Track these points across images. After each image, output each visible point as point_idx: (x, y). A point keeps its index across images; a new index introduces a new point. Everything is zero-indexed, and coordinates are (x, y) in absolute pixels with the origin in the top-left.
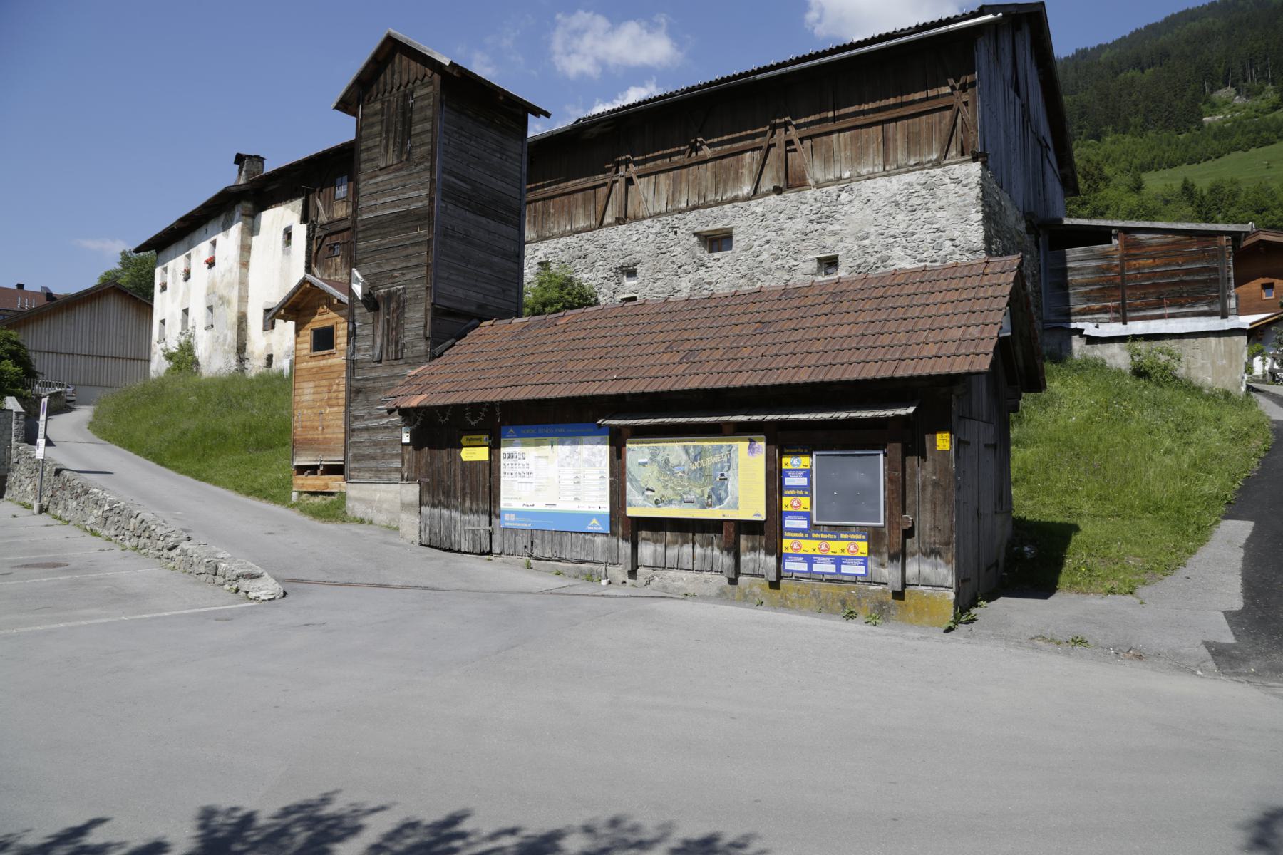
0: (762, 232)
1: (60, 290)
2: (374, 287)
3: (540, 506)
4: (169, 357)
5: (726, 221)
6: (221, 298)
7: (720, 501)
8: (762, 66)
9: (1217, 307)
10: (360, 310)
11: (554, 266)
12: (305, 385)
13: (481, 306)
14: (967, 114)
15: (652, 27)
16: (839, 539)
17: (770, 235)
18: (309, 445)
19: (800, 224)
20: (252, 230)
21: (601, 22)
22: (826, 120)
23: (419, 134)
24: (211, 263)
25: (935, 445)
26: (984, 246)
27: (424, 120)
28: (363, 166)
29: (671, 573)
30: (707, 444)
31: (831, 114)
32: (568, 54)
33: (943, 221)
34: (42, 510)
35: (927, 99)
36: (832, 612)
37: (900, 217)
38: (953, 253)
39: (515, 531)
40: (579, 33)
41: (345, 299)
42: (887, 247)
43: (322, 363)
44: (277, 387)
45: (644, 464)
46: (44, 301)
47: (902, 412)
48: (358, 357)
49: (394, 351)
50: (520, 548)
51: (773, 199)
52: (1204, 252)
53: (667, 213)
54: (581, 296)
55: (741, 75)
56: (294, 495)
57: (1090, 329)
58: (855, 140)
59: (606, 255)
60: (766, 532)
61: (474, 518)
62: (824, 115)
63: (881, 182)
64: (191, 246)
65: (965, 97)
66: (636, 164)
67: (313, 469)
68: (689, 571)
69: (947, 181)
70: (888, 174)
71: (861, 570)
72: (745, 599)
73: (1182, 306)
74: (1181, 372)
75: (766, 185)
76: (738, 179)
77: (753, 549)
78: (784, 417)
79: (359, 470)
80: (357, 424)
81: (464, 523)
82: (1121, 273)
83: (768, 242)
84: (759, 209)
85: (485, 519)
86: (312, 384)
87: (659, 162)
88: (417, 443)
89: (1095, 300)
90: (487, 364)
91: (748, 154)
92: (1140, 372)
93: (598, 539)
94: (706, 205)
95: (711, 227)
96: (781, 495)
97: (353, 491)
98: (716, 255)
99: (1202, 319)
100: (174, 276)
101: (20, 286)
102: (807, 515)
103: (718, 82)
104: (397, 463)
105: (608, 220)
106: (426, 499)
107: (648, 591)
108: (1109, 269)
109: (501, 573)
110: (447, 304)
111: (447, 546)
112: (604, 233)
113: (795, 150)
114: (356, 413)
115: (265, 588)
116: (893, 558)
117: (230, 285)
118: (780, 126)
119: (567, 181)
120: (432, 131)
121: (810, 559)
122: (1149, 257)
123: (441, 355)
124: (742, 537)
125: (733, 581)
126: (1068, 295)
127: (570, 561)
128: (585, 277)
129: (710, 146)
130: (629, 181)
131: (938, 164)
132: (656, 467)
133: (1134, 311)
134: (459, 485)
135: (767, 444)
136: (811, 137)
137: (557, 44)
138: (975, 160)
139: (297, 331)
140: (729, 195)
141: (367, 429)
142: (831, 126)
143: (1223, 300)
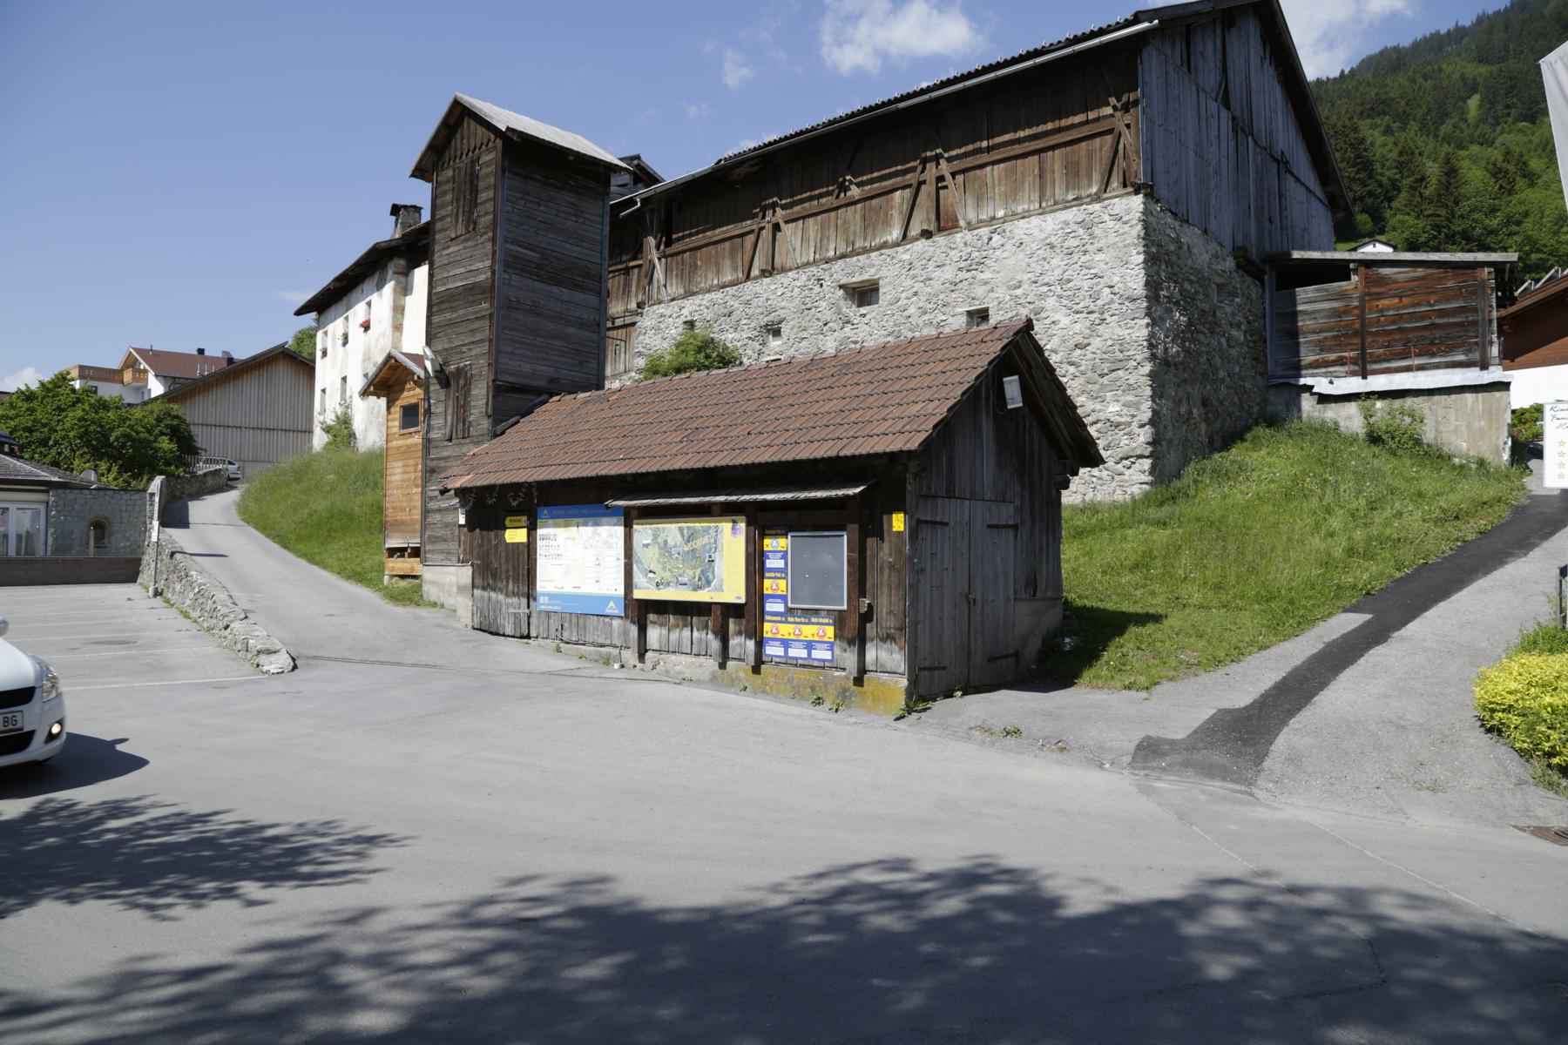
0: (909, 282)
2: (446, 363)
3: (568, 589)
5: (873, 271)
7: (708, 583)
8: (1079, 33)
9: (1476, 356)
11: (698, 324)
13: (552, 380)
14: (1128, 138)
17: (918, 286)
18: (400, 526)
19: (949, 273)
20: (405, 289)
23: (483, 203)
24: (366, 326)
25: (891, 525)
26: (1144, 293)
27: (487, 188)
29: (673, 657)
30: (698, 525)
31: (985, 144)
32: (840, 45)
34: (157, 593)
36: (803, 698)
37: (1054, 262)
38: (1112, 302)
39: (548, 614)
42: (1041, 296)
45: (647, 546)
48: (433, 435)
49: (461, 430)
50: (552, 631)
51: (922, 244)
52: (1460, 288)
53: (815, 262)
55: (884, 104)
57: (1322, 385)
59: (749, 312)
60: (745, 615)
61: (515, 600)
62: (977, 145)
64: (349, 308)
65: (1128, 119)
66: (784, 207)
67: (400, 552)
68: (684, 653)
69: (1106, 218)
71: (827, 655)
72: (732, 684)
73: (1433, 355)
74: (1429, 436)
75: (915, 230)
76: (887, 223)
77: (739, 633)
78: (734, 498)
80: (432, 505)
82: (1362, 317)
83: (916, 294)
84: (906, 257)
85: (524, 601)
86: (400, 464)
87: (807, 205)
88: (471, 525)
89: (1330, 350)
91: (898, 193)
92: (1374, 439)
93: (616, 622)
94: (855, 253)
95: (858, 278)
96: (762, 577)
97: (428, 574)
98: (863, 310)
99: (1458, 371)
100: (334, 341)
101: (201, 351)
102: (784, 598)
104: (453, 546)
105: (755, 272)
106: (478, 581)
107: (654, 675)
108: (1346, 311)
109: (536, 657)
110: (511, 379)
111: (493, 629)
112: (749, 286)
113: (946, 187)
116: (851, 642)
118: (931, 159)
119: (714, 228)
121: (786, 644)
122: (1394, 296)
123: (503, 433)
124: (731, 621)
125: (722, 666)
126: (1297, 345)
127: (593, 644)
128: (730, 338)
129: (859, 185)
130: (777, 228)
131: (1097, 198)
132: (656, 550)
133: (1375, 362)
135: (748, 525)
136: (964, 171)
137: (826, 37)
138: (1137, 192)
139: (388, 408)
140: (877, 241)
141: (440, 510)
142: (985, 158)
143: (1484, 346)
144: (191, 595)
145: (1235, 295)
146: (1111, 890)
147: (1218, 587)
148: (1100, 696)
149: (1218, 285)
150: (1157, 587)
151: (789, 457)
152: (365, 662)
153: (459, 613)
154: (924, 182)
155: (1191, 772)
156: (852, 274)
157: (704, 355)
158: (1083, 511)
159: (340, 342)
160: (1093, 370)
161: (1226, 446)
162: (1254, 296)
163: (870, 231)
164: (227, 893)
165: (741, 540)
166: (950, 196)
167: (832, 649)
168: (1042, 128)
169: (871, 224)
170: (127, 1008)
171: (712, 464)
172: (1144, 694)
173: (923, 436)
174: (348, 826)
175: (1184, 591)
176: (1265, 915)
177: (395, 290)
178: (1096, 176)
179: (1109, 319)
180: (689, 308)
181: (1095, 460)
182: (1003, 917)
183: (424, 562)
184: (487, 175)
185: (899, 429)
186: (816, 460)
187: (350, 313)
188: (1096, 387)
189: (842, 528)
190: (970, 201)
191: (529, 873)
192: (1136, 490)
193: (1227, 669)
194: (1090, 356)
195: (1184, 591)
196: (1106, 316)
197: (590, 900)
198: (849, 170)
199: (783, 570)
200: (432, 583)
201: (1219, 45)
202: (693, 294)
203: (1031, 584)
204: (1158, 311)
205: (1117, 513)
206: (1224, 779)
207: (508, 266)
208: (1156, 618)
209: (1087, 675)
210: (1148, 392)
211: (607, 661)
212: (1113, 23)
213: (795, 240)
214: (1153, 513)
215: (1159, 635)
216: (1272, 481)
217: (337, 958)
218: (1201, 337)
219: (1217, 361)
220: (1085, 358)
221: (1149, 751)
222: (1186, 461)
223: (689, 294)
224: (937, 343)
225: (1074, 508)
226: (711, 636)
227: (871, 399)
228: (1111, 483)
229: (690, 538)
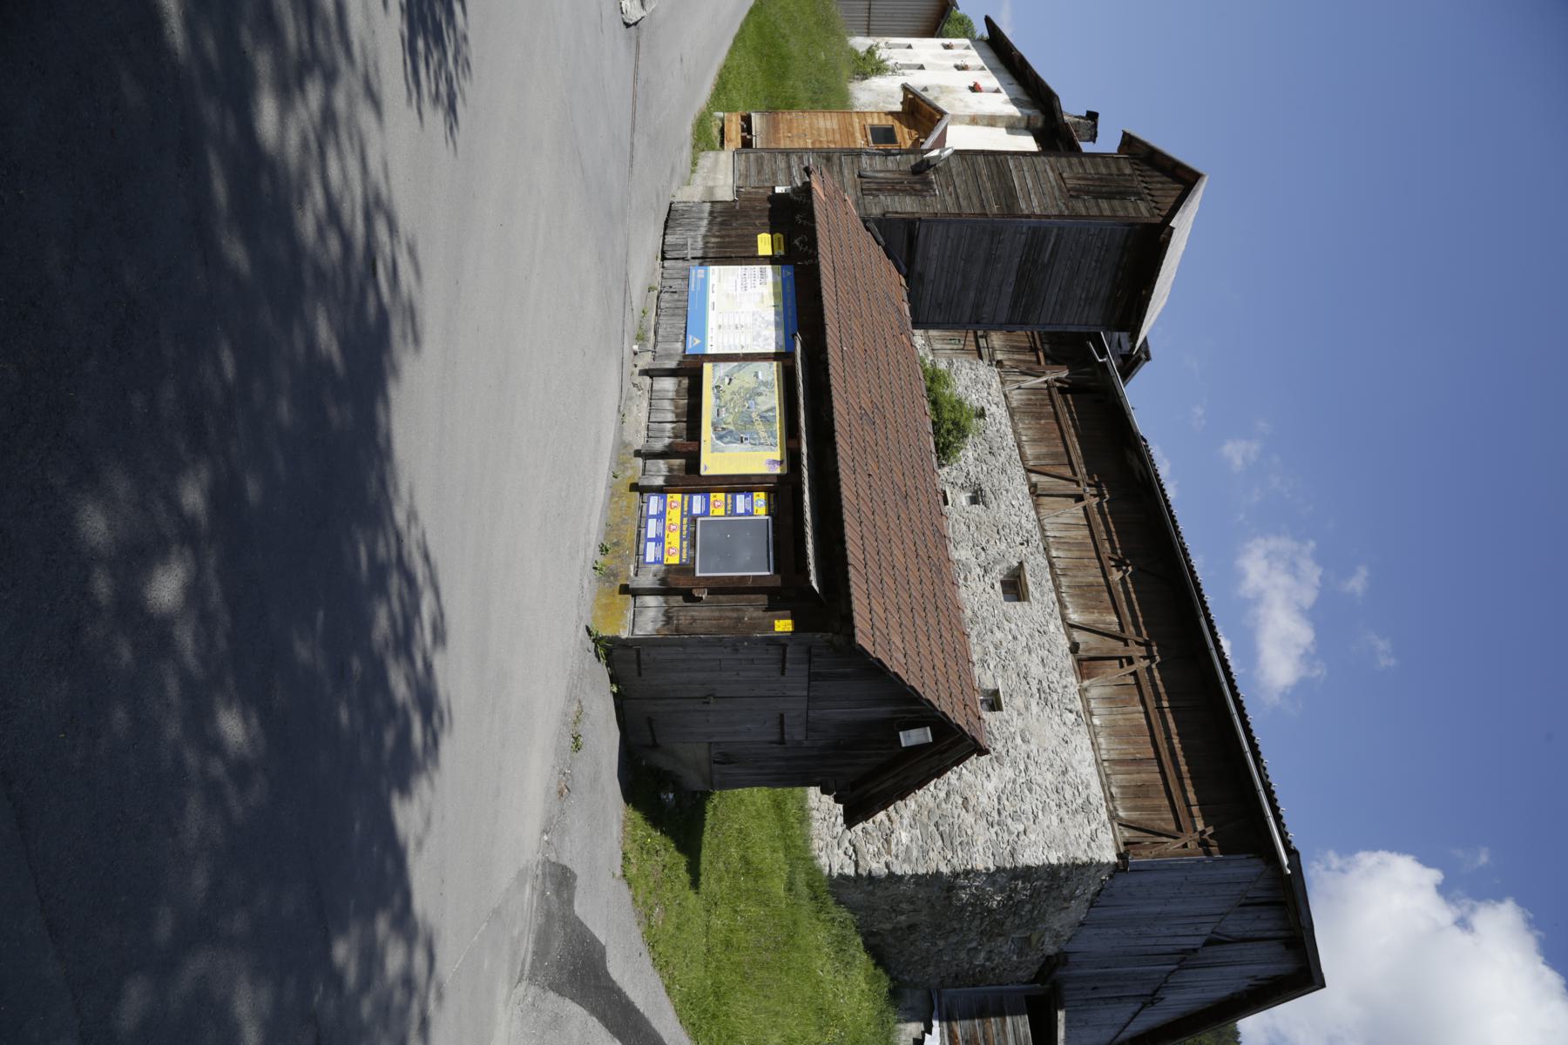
0: (1026, 632)
2: (937, 171)
3: (712, 298)
5: (1037, 595)
7: (720, 438)
8: (1276, 796)
11: (981, 422)
12: (835, 121)
13: (921, 277)
14: (1173, 846)
15: (1307, 658)
16: (682, 539)
18: (773, 127)
19: (1036, 671)
20: (1012, 127)
21: (1309, 597)
24: (975, 89)
25: (780, 618)
26: (1019, 865)
27: (1113, 209)
28: (1064, 160)
29: (645, 404)
30: (778, 427)
31: (1165, 704)
33: (1046, 823)
35: (1189, 806)
36: (607, 535)
37: (1049, 775)
38: (1010, 833)
39: (687, 278)
40: (1293, 569)
41: (925, 147)
42: (1014, 763)
43: (858, 135)
44: (831, 97)
45: (756, 375)
47: (814, 584)
48: (865, 160)
49: (869, 187)
50: (670, 283)
51: (1065, 644)
56: (721, 114)
58: (1137, 729)
59: (995, 473)
61: (700, 244)
62: (1164, 697)
63: (1090, 755)
65: (1192, 845)
66: (1099, 505)
67: (747, 128)
68: (649, 414)
69: (1094, 826)
71: (650, 558)
72: (621, 463)
75: (1078, 636)
76: (1086, 608)
77: (671, 470)
80: (794, 159)
81: (694, 237)
83: (1015, 638)
84: (1052, 628)
85: (699, 253)
88: (775, 199)
90: (857, 273)
93: (679, 346)
94: (1055, 577)
95: (1029, 580)
96: (727, 491)
97: (725, 157)
98: (998, 586)
100: (960, 56)
102: (706, 513)
103: (1195, 579)
104: (753, 181)
105: (1034, 478)
106: (718, 207)
107: (627, 385)
109: (644, 268)
111: (670, 223)
113: (1122, 666)
116: (663, 581)
118: (1149, 650)
121: (661, 516)
123: (868, 229)
124: (683, 461)
125: (638, 454)
126: (972, 1018)
127: (657, 324)
128: (968, 454)
129: (1123, 579)
130: (1079, 498)
131: (1113, 817)
132: (753, 385)
134: (733, 233)
135: (778, 476)
136: (1138, 684)
137: (1284, 544)
138: (1119, 855)
139: (891, 113)
140: (1067, 599)
141: (789, 167)
142: (1151, 705)
145: (1020, 953)
147: (728, 944)
148: (616, 829)
150: (726, 883)
151: (846, 516)
152: (635, 96)
153: (686, 188)
155: (541, 920)
156: (1033, 575)
157: (950, 427)
158: (802, 808)
159: (959, 63)
160: (942, 816)
161: (870, 948)
163: (1078, 592)
166: (1113, 671)
167: (656, 562)
168: (1182, 760)
169: (1084, 593)
171: (838, 439)
172: (619, 873)
174: (466, 85)
175: (724, 909)
176: (398, 996)
177: (1011, 117)
178: (1135, 815)
179: (993, 831)
180: (998, 413)
181: (851, 820)
182: (389, 738)
183: (737, 152)
184: (1126, 208)
185: (879, 625)
187: (988, 72)
188: (925, 820)
189: (777, 570)
190: (1108, 691)
192: (824, 861)
193: (645, 954)
194: (956, 812)
195: (724, 909)
196: (996, 828)
197: (396, 329)
198: (1137, 570)
199: (734, 512)
200: (716, 161)
201: (1268, 934)
202: (1012, 416)
203: (726, 759)
205: (800, 843)
206: (535, 953)
207: (1034, 231)
208: (695, 883)
209: (637, 816)
210: (921, 871)
211: (640, 338)
212: (1287, 829)
213: (1067, 517)
214: (801, 879)
215: (678, 886)
216: (835, 995)
217: (330, 78)
218: (977, 922)
220: (953, 808)
221: (561, 879)
222: (853, 909)
223: (1012, 412)
225: (804, 799)
226: (667, 441)
227: (906, 596)
228: (830, 837)
229: (765, 419)
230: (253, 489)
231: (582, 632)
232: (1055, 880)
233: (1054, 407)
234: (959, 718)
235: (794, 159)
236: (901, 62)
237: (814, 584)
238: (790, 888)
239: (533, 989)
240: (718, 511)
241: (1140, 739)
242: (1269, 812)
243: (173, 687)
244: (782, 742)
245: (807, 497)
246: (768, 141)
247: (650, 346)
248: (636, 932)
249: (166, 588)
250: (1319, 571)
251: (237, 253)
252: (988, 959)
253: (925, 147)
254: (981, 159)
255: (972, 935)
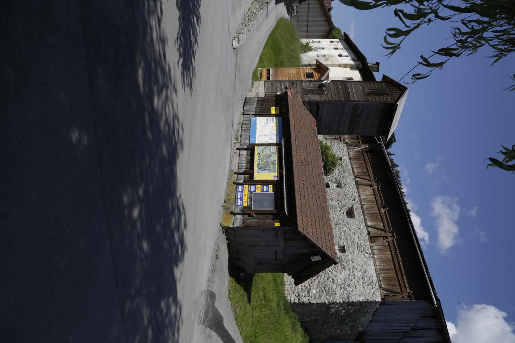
0: (354, 228)
1: (332, 12)
2: (326, 87)
3: (258, 127)
4: (307, 44)
5: (357, 216)
6: (328, 59)
7: (259, 169)
8: (433, 281)
10: (318, 83)
11: (340, 162)
14: (399, 297)
15: (456, 237)
18: (276, 73)
19: (357, 240)
20: (352, 68)
21: (456, 216)
22: (396, 250)
24: (340, 55)
25: (276, 222)
27: (379, 99)
29: (238, 158)
30: (276, 166)
31: (398, 252)
33: (359, 288)
35: (405, 284)
36: (226, 197)
37: (360, 273)
38: (347, 291)
39: (250, 120)
40: (450, 207)
41: (322, 79)
43: (302, 75)
46: (327, 8)
47: (286, 211)
48: (304, 83)
49: (305, 92)
51: (366, 232)
53: (360, 198)
54: (330, 169)
60: (250, 180)
61: (254, 110)
62: (397, 249)
63: (373, 267)
65: (406, 297)
66: (378, 188)
67: (268, 73)
68: (239, 162)
69: (374, 290)
70: (376, 270)
71: (239, 204)
72: (230, 176)
75: (370, 229)
76: (373, 221)
77: (245, 178)
79: (268, 84)
80: (282, 83)
81: (252, 108)
83: (350, 230)
84: (362, 227)
85: (254, 113)
88: (277, 96)
90: (301, 118)
93: (248, 141)
94: (363, 211)
95: (355, 212)
96: (261, 185)
98: (345, 213)
100: (336, 45)
102: (255, 191)
105: (357, 179)
106: (260, 99)
107: (233, 153)
109: (238, 117)
112: (352, 177)
114: (286, 83)
115: (235, 43)
116: (242, 211)
117: (332, 61)
118: (393, 234)
119: (371, 166)
120: (376, 101)
121: (242, 192)
124: (248, 176)
125: (235, 173)
127: (241, 134)
128: (336, 171)
129: (385, 212)
130: (371, 186)
131: (380, 287)
135: (276, 180)
136: (389, 245)
138: (382, 299)
140: (367, 218)
141: (281, 86)
142: (393, 252)
144: (255, 11)
145: (351, 330)
146: (179, 280)
147: (259, 321)
148: (227, 283)
149: (354, 326)
150: (259, 303)
151: (296, 193)
152: (236, 68)
153: (250, 93)
154: (386, 232)
155: (206, 307)
156: (356, 210)
157: (329, 164)
158: (282, 281)
161: (302, 326)
162: (351, 337)
164: (180, 56)
165: (272, 178)
166: (381, 241)
167: (240, 205)
168: (403, 269)
169: (373, 217)
170: (159, 45)
171: (294, 170)
172: (227, 296)
173: (302, 231)
174: (194, 80)
175: (257, 311)
176: (173, 319)
177: (351, 65)
178: (387, 287)
180: (346, 159)
181: (296, 283)
182: (174, 251)
183: (265, 81)
184: (383, 99)
185: (305, 225)
186: (295, 200)
187: (344, 50)
189: (275, 208)
190: (379, 247)
191: (184, 130)
192: (289, 298)
193: (234, 321)
194: (330, 284)
195: (257, 311)
196: (343, 289)
197: (178, 146)
199: (263, 191)
200: (259, 84)
201: (432, 327)
202: (350, 160)
203: (260, 264)
204: (344, 306)
205: (281, 292)
206: (204, 316)
208: (249, 301)
209: (233, 280)
210: (319, 302)
211: (236, 139)
212: (436, 292)
213: (367, 192)
214: (281, 303)
215: (244, 302)
216: (292, 341)
217: (167, 88)
218: (337, 319)
219: (330, 325)
220: (330, 282)
221: (212, 296)
222: (298, 313)
223: (350, 159)
224: (331, 236)
225: (283, 278)
226: (244, 170)
227: (313, 216)
228: (293, 291)
229: (273, 164)
230: (151, 189)
231: (219, 225)
232: (362, 307)
233: (364, 157)
234: (329, 253)
235: (282, 83)
236: (317, 47)
237: (286, 213)
238: (278, 305)
239: (204, 326)
240: (259, 191)
241: (390, 263)
242: (430, 287)
243: (136, 235)
244: (276, 259)
245: (285, 187)
246: (275, 77)
247: (239, 141)
248: (232, 314)
249: (136, 213)
250: (459, 208)
251: (150, 135)
252: (341, 332)
253: (322, 79)
254: (339, 83)
255: (335, 324)
